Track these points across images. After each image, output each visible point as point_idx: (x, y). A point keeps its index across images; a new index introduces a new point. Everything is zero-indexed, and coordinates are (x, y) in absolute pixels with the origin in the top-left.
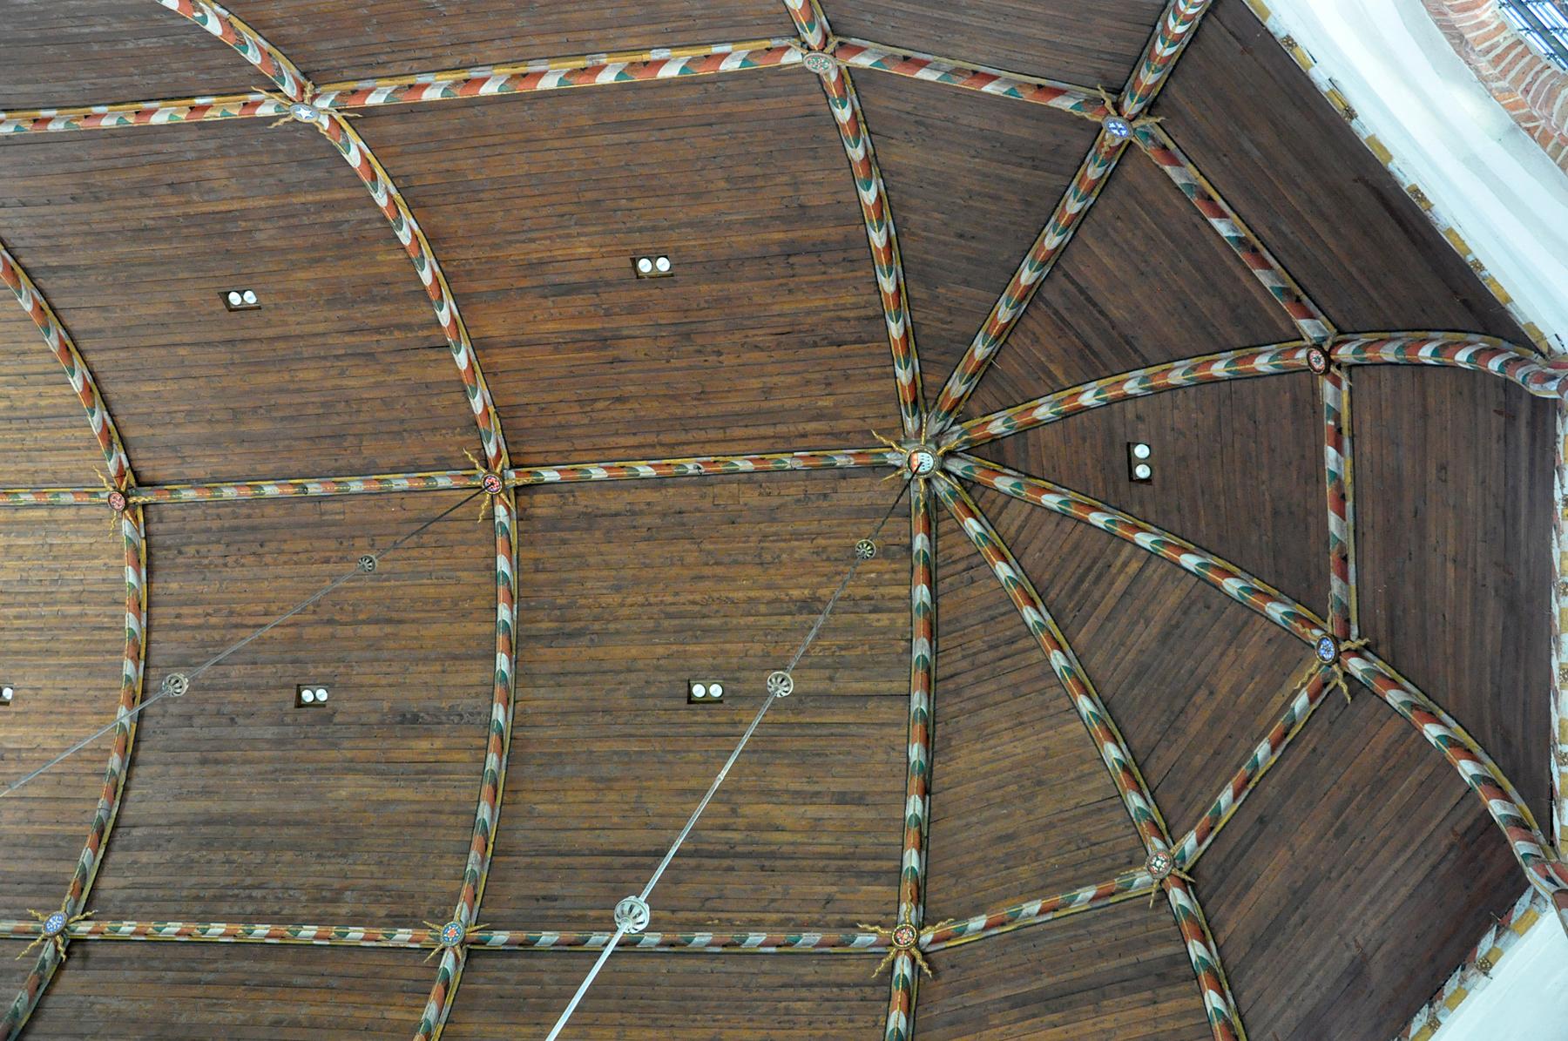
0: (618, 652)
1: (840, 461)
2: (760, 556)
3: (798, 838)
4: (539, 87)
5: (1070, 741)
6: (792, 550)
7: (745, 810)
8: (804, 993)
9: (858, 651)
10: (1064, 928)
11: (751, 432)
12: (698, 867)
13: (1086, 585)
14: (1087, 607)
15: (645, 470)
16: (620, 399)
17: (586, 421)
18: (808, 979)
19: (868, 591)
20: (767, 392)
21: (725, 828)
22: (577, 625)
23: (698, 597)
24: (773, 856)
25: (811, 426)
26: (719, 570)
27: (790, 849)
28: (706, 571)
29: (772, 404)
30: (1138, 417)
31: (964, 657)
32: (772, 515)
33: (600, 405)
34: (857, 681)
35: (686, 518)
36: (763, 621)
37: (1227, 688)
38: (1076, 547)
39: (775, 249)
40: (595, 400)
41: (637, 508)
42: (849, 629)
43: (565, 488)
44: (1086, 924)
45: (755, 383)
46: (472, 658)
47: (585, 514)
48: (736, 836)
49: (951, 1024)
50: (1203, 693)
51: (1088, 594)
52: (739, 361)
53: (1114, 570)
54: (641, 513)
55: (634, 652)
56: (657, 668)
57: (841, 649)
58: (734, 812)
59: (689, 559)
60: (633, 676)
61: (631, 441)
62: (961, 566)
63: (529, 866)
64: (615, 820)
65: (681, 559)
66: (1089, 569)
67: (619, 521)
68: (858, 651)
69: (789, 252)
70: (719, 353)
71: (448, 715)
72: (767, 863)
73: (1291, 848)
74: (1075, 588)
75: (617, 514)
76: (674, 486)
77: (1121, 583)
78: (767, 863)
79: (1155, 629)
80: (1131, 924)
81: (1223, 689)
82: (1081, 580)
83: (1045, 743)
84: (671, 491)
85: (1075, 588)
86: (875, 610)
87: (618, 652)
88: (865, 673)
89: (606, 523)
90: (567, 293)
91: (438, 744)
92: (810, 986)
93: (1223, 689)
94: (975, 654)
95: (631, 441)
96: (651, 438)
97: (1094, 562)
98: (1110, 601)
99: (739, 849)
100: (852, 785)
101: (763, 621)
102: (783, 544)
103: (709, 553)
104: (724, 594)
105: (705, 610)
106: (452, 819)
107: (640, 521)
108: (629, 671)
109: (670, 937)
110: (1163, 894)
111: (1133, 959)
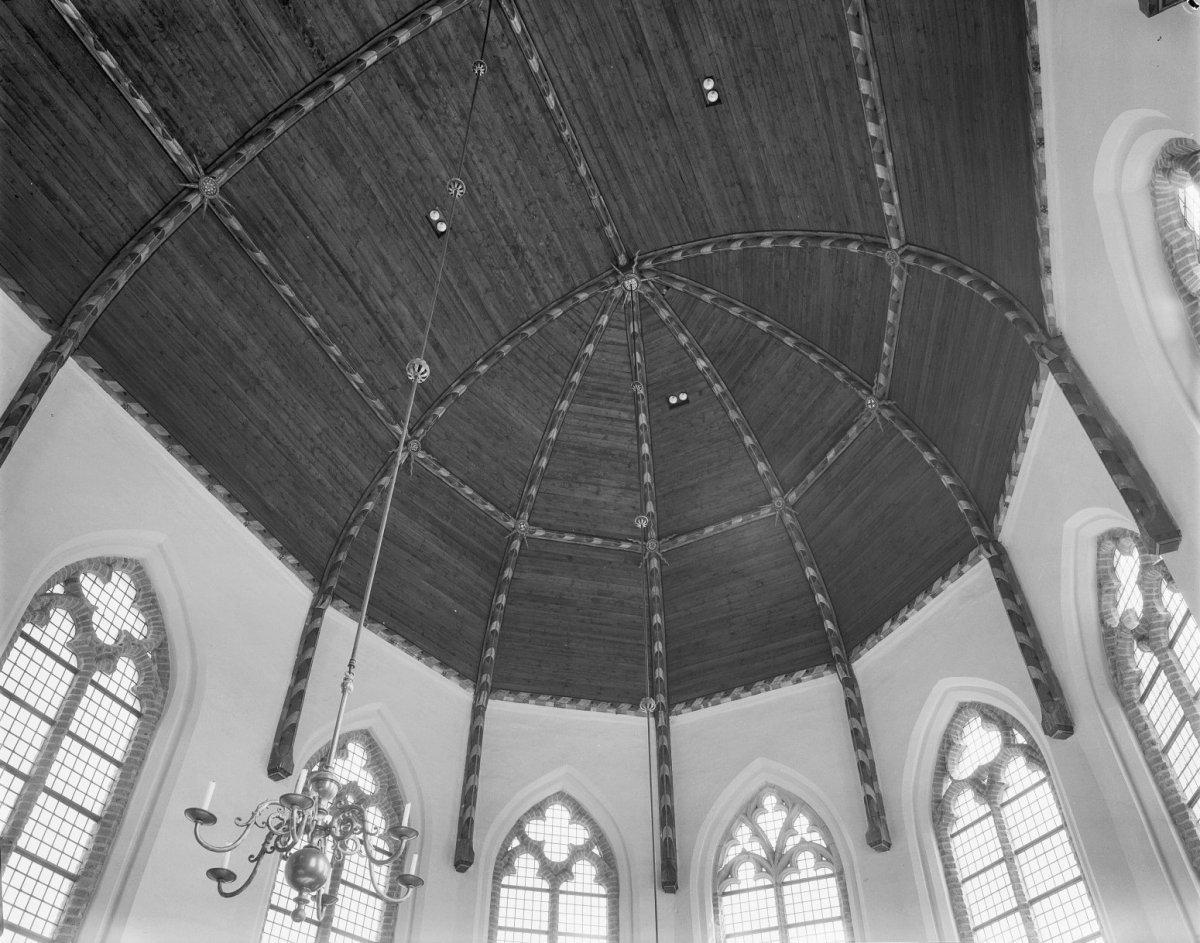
0: (424, 142)
1: (608, 229)
2: (530, 204)
3: (406, 343)
4: (860, 80)
5: (532, 435)
6: (543, 222)
7: (399, 303)
8: (354, 423)
9: (509, 295)
10: (469, 509)
11: (606, 166)
12: (355, 303)
13: (603, 394)
14: (595, 401)
15: (551, 100)
16: (596, 67)
17: (569, 41)
18: (361, 419)
19: (541, 279)
20: (637, 171)
21: (382, 298)
22: (424, 98)
23: (487, 178)
24: (389, 338)
25: (623, 201)
26: (510, 182)
27: (398, 343)
28: (505, 174)
29: (629, 175)
30: (700, 392)
31: (536, 353)
32: (557, 197)
33: (585, 50)
34: (494, 306)
35: (531, 140)
36: (495, 229)
37: (604, 500)
38: (618, 379)
39: (742, 175)
40: (588, 46)
41: (521, 101)
42: (518, 282)
43: (512, 38)
44: (477, 515)
45: (640, 163)
46: (355, 21)
47: (499, 60)
48: (383, 309)
49: (402, 502)
50: (595, 488)
51: (599, 397)
52: (654, 152)
53: (618, 405)
54: (519, 105)
55: (432, 155)
56: (433, 179)
57: (505, 284)
58: (392, 297)
59: (506, 157)
60: (416, 163)
61: (567, 80)
62: (578, 321)
63: (274, 192)
64: (339, 226)
65: (504, 152)
66: (612, 392)
67: (507, 91)
68: (509, 295)
69: (744, 186)
70: (655, 137)
71: (305, 31)
72: (384, 339)
73: (573, 581)
74: (599, 389)
75: (510, 87)
76: (548, 122)
77: (614, 413)
78: (384, 339)
79: (605, 444)
80: (491, 533)
81: (601, 499)
82: (606, 391)
83: (524, 424)
84: (543, 120)
85: (599, 389)
86: (534, 289)
87: (424, 142)
88: (499, 306)
89: (501, 82)
90: (671, 21)
91: (284, 39)
92: (358, 422)
93: (601, 499)
94: (541, 358)
95: (567, 80)
96: (574, 94)
97: (617, 393)
98: (603, 412)
99: (379, 317)
100: (443, 342)
101: (495, 229)
102: (543, 213)
103: (517, 169)
104: (497, 194)
105: (482, 188)
106: (250, 99)
107: (514, 107)
108: (420, 161)
109: (321, 331)
110: (514, 537)
111: (483, 549)
